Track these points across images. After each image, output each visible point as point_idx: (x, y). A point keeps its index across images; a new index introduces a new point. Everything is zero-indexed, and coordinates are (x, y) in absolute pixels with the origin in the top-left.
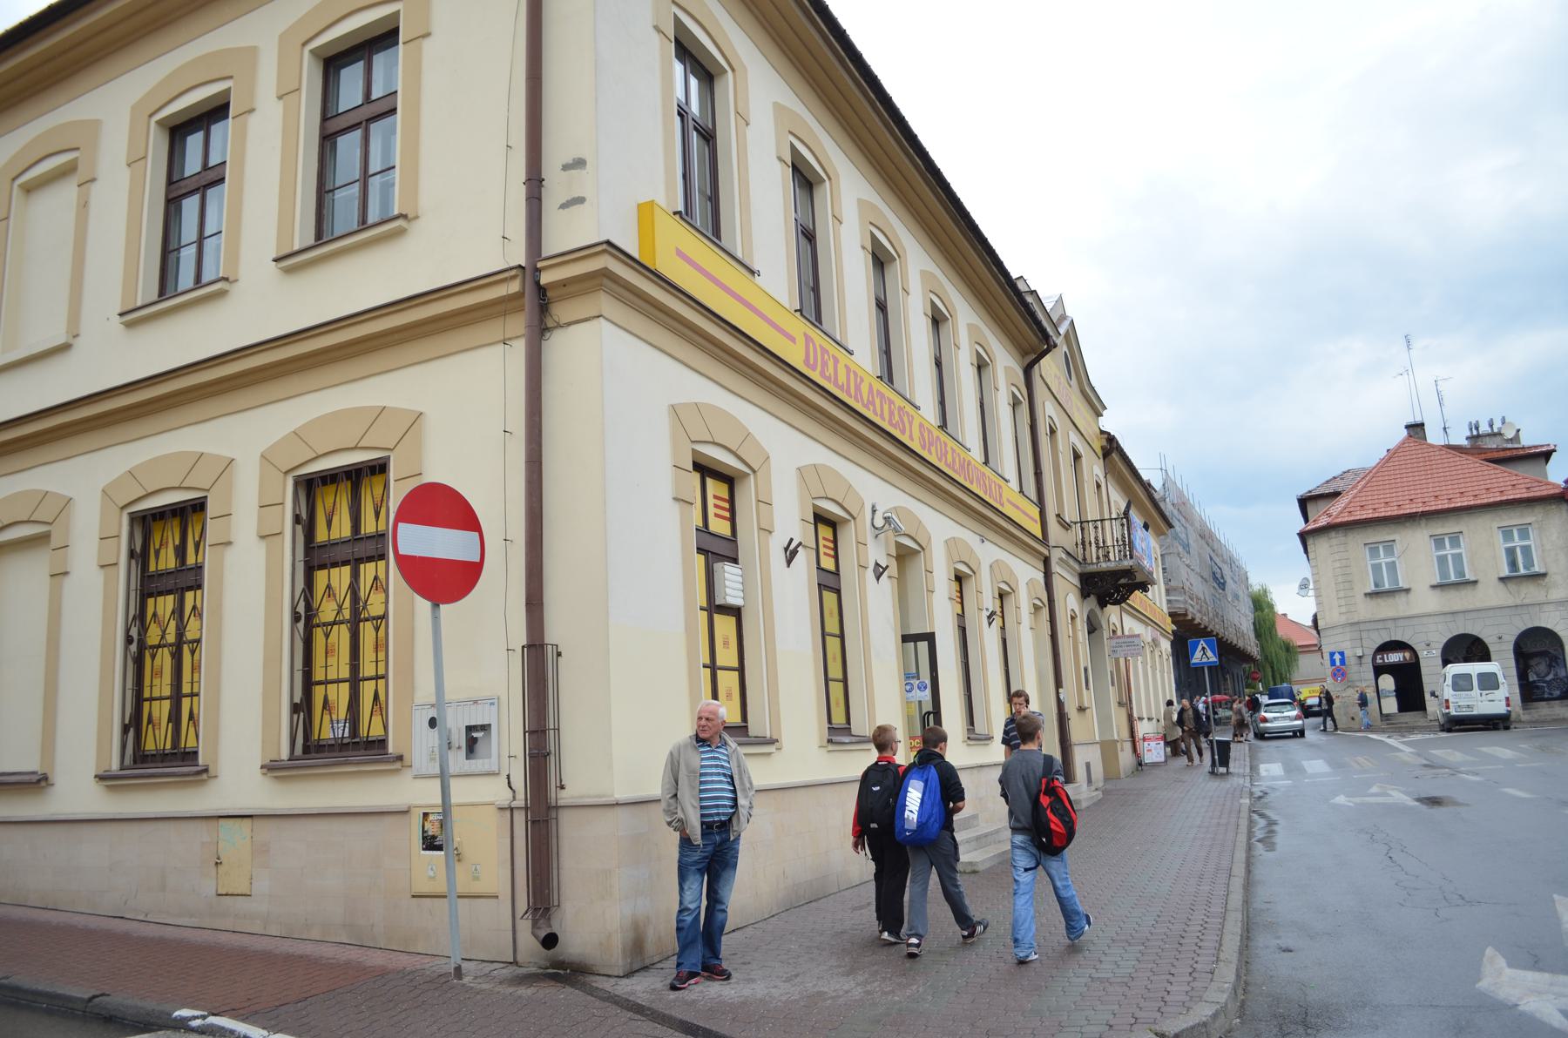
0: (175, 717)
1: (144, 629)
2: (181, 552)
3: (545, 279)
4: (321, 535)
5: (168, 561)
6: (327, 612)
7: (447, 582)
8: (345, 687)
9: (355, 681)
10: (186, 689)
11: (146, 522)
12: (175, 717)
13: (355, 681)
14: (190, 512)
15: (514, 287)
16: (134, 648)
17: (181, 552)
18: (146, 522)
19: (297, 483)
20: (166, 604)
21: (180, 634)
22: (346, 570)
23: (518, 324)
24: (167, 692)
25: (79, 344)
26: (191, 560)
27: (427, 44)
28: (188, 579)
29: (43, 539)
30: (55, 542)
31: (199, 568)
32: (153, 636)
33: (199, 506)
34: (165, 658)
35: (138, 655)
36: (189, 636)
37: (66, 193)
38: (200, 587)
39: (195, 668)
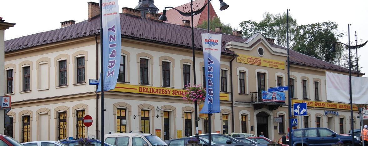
0: (82, 135)
1: (24, 129)
2: (64, 117)
3: (98, 94)
4: (79, 117)
5: (26, 122)
6: (79, 125)
7: (89, 125)
8: (81, 134)
9: (82, 133)
10: (65, 133)
11: (60, 114)
12: (82, 135)
13: (82, 133)
14: (65, 113)
15: (95, 94)
16: (23, 131)
17: (64, 117)
18: (60, 114)
19: (22, 117)
20: (81, 122)
21: (64, 127)
22: (81, 121)
23: (96, 97)
24: (81, 132)
25: (50, 89)
26: (65, 118)
27: (69, 64)
28: (65, 120)
29: (47, 114)
30: (48, 115)
31: (66, 119)
32: (25, 130)
33: (84, 110)
34: (62, 130)
35: (23, 132)
36: (65, 127)
37: (46, 66)
38: (66, 121)
39: (66, 131)
